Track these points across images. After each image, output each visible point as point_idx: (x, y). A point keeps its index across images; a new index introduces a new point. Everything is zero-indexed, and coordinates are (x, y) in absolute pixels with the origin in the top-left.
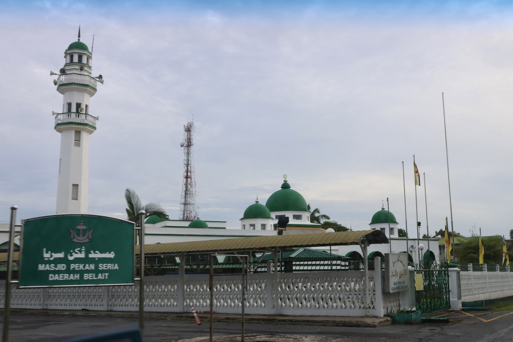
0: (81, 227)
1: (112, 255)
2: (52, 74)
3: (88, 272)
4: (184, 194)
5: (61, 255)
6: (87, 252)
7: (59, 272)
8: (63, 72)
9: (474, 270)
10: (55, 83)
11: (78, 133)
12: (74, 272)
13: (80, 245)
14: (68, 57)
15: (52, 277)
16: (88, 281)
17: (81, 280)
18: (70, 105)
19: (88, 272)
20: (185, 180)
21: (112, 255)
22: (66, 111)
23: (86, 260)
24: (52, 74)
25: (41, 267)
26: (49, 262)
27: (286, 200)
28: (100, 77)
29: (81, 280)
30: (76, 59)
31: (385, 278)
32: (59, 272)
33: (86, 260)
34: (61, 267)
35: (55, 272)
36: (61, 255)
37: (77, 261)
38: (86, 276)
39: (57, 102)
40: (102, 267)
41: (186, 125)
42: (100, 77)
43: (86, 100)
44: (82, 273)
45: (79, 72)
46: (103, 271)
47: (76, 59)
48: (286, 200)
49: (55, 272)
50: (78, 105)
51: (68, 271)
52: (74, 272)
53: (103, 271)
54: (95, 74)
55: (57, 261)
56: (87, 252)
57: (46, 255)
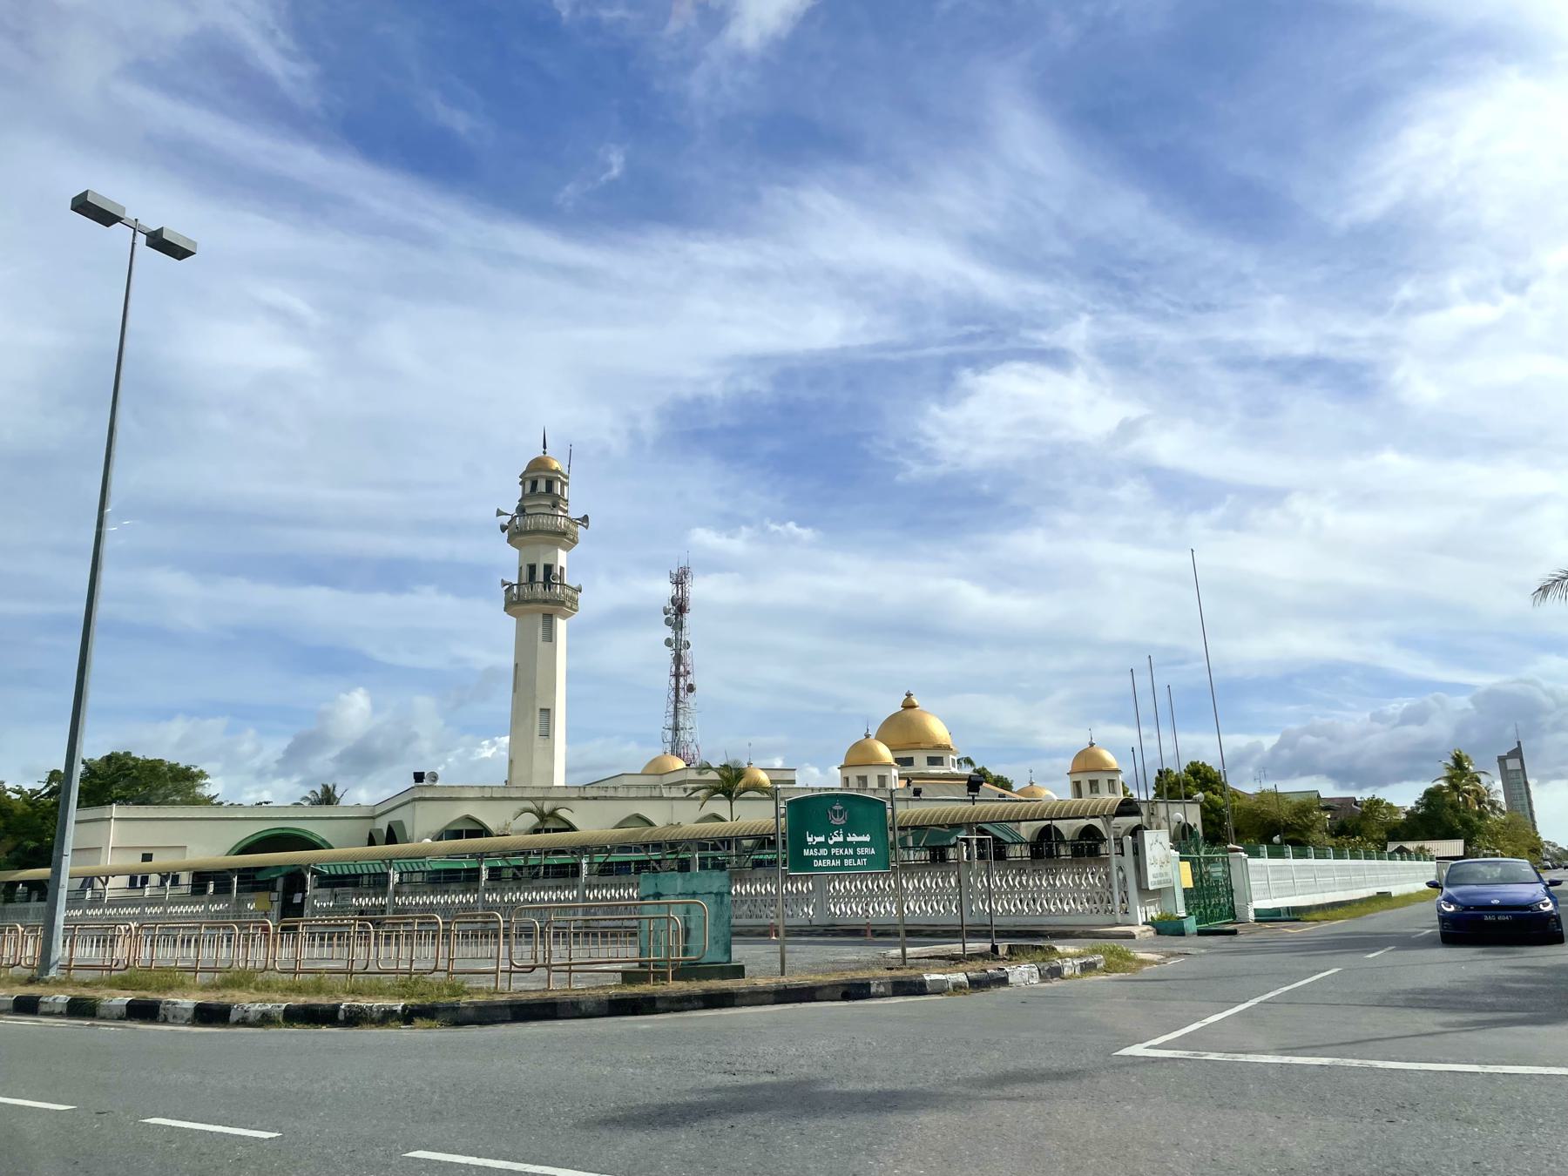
0: (838, 807)
1: (867, 839)
2: (499, 513)
3: (848, 857)
4: (671, 708)
5: (822, 839)
6: (845, 836)
7: (822, 858)
8: (521, 510)
9: (1271, 856)
10: (503, 528)
11: (549, 619)
12: (835, 857)
13: (837, 827)
14: (528, 485)
15: (817, 863)
16: (849, 868)
17: (842, 867)
18: (532, 568)
19: (848, 857)
20: (673, 681)
21: (867, 839)
22: (525, 579)
23: (845, 844)
24: (499, 513)
25: (806, 853)
26: (812, 847)
27: (902, 727)
28: (586, 518)
29: (842, 867)
30: (542, 487)
31: (1140, 868)
32: (822, 858)
33: (845, 844)
34: (824, 852)
35: (818, 858)
36: (822, 839)
37: (837, 845)
38: (847, 862)
39: (508, 560)
40: (860, 851)
41: (675, 571)
42: (586, 518)
43: (562, 558)
44: (842, 858)
45: (548, 511)
46: (861, 857)
47: (542, 487)
48: (902, 727)
49: (818, 858)
50: (548, 569)
51: (830, 857)
52: (835, 857)
53: (861, 857)
54: (575, 512)
55: (819, 845)
56: (845, 836)
57: (810, 839)
